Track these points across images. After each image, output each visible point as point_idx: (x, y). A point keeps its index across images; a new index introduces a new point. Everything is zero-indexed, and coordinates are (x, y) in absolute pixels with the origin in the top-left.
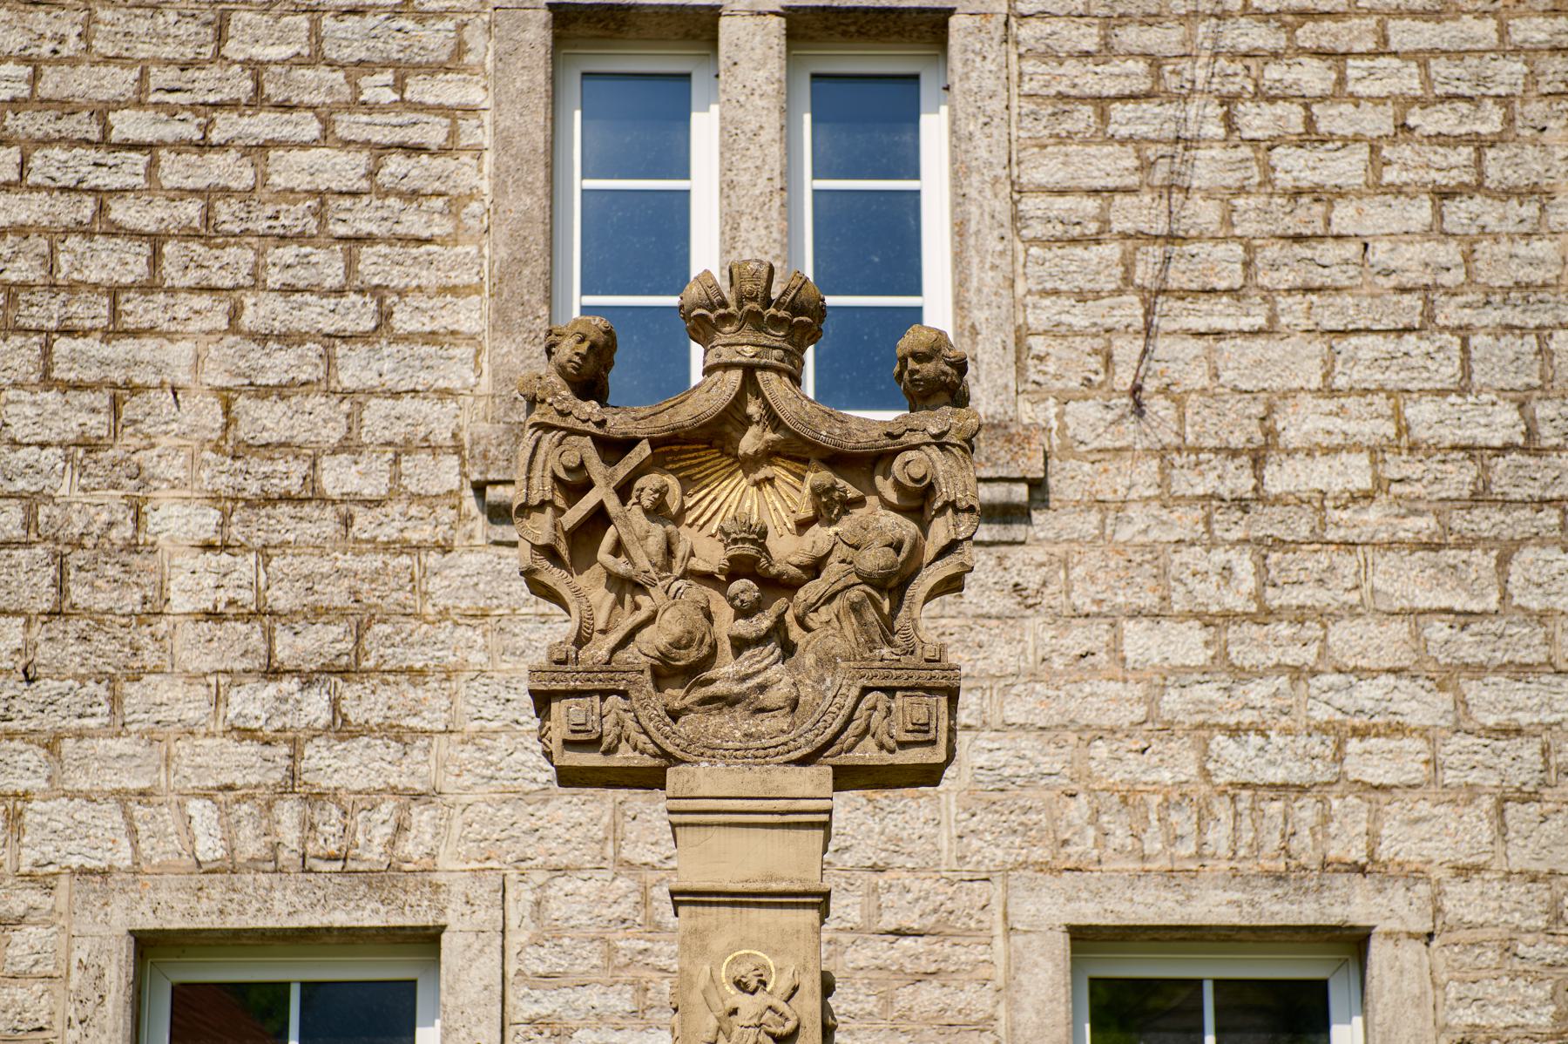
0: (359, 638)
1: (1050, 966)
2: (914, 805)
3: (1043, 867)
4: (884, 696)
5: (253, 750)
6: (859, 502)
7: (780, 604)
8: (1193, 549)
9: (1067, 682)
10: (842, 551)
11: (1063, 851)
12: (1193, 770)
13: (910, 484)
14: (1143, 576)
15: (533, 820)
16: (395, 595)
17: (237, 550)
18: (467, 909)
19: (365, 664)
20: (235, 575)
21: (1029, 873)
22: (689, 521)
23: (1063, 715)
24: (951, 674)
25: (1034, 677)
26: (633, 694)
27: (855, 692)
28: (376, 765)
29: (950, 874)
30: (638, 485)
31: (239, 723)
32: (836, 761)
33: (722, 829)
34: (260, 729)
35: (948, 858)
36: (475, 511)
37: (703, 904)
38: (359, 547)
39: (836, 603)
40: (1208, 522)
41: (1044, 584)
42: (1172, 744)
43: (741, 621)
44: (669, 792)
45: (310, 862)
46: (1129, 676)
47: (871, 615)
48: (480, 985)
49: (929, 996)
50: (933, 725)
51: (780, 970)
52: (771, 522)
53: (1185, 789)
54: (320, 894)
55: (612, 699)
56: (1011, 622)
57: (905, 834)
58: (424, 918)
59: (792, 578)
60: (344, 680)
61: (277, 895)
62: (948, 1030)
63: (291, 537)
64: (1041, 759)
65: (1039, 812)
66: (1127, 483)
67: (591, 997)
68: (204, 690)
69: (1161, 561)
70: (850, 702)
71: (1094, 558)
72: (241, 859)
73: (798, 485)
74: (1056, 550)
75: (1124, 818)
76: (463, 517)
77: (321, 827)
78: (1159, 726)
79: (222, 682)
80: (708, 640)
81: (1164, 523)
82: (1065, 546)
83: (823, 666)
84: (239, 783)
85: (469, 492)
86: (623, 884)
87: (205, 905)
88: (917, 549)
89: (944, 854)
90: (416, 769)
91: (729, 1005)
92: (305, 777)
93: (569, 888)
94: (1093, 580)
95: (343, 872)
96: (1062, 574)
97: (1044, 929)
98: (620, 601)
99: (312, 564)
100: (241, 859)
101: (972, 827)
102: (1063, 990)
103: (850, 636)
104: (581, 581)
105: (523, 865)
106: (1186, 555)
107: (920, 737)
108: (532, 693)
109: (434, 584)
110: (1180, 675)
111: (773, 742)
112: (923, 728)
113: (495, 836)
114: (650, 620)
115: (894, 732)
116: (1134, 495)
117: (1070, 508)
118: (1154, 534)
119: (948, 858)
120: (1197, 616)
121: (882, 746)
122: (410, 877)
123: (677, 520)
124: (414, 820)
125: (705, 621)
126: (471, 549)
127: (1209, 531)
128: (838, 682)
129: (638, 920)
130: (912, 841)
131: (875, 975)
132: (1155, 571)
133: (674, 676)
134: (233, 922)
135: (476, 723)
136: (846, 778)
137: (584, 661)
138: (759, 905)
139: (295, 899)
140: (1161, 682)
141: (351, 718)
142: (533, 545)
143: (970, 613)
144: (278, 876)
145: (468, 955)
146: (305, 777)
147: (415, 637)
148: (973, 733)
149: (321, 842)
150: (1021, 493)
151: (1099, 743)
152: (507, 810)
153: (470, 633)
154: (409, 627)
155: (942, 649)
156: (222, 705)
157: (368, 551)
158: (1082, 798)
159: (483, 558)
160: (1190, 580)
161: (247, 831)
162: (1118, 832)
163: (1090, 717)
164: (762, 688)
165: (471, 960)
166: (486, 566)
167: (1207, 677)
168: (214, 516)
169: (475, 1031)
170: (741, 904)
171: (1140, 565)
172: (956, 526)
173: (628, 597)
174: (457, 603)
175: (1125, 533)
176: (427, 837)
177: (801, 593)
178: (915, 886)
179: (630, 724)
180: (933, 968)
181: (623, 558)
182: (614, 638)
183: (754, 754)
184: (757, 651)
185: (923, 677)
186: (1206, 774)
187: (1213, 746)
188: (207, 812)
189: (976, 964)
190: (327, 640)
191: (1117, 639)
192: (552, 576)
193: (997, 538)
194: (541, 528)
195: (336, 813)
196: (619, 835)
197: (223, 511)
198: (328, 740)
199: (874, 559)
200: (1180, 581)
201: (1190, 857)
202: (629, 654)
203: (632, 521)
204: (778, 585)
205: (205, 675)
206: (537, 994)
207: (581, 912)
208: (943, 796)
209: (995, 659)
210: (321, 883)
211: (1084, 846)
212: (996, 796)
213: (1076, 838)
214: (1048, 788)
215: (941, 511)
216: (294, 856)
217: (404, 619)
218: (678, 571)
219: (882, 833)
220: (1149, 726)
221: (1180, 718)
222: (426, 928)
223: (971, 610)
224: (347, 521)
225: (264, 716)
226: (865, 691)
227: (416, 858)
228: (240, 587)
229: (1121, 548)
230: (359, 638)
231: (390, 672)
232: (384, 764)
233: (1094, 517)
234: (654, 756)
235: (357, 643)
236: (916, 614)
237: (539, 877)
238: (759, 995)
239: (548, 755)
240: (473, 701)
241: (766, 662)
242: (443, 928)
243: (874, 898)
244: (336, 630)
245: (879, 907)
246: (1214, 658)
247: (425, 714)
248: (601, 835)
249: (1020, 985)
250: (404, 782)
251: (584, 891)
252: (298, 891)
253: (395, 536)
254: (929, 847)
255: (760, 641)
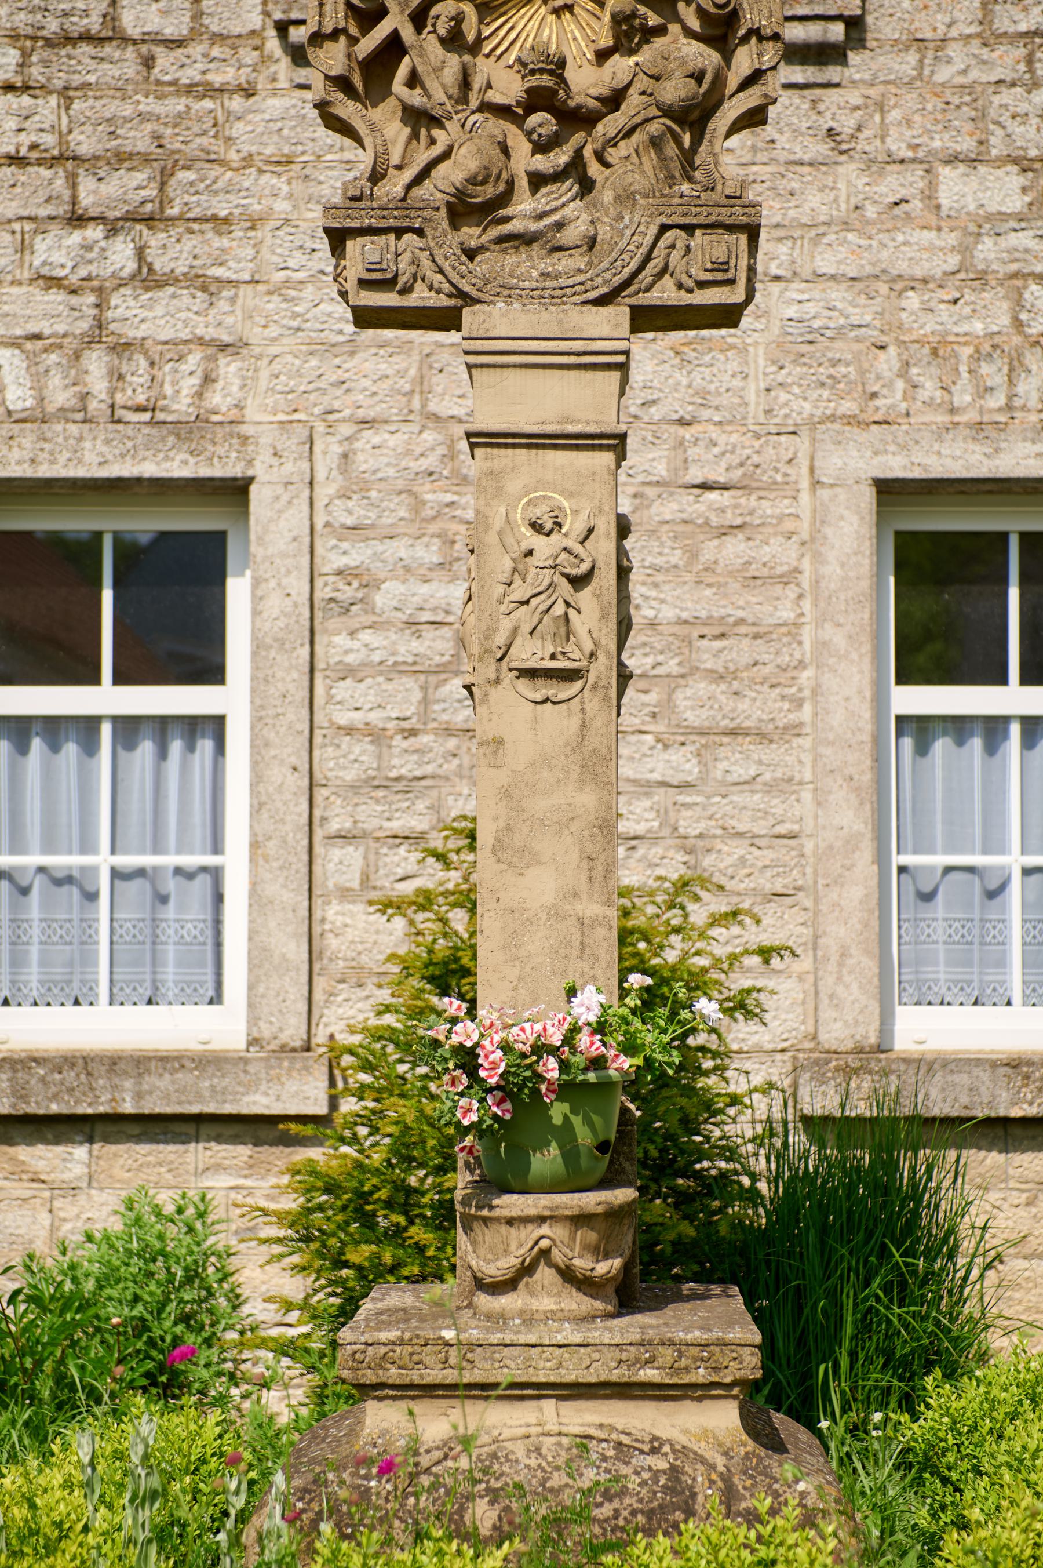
0: (163, 184)
1: (855, 519)
2: (721, 357)
3: (851, 420)
4: (683, 234)
5: (60, 298)
6: (661, 31)
7: (579, 137)
8: (1013, 90)
9: (880, 231)
10: (643, 82)
11: (871, 404)
12: (1005, 320)
13: (713, 10)
14: (960, 121)
15: (340, 372)
16: (198, 140)
17: (38, 92)
18: (275, 461)
19: (170, 212)
20: (37, 118)
21: (837, 426)
22: (486, 51)
23: (874, 265)
24: (752, 211)
25: (846, 226)
26: (429, 232)
27: (654, 230)
28: (183, 315)
29: (756, 428)
30: (433, 12)
31: (45, 271)
32: (633, 301)
33: (518, 371)
34: (66, 277)
35: (755, 411)
36: (278, 52)
37: (499, 445)
38: (161, 89)
39: (636, 138)
40: (1030, 60)
41: (859, 129)
42: (985, 295)
43: (539, 156)
44: (464, 332)
45: (120, 413)
46: (943, 224)
47: (671, 150)
48: (288, 536)
49: (734, 548)
50: (732, 264)
51: (576, 512)
52: (571, 52)
53: (997, 340)
54: (129, 444)
55: (408, 237)
56: (824, 168)
57: (712, 387)
58: (235, 470)
59: (590, 111)
60: (150, 228)
61: (87, 444)
62: (752, 583)
63: (92, 78)
64: (851, 310)
65: (848, 365)
66: (948, 20)
67: (399, 549)
68: (8, 237)
69: (980, 102)
70: (648, 240)
71: (910, 100)
72: (50, 408)
73: (598, 12)
74: (872, 92)
75: (934, 370)
76: (267, 59)
77: (129, 378)
78: (972, 276)
79: (27, 228)
80: (504, 176)
81: (984, 62)
82: (881, 88)
83: (621, 206)
84: (47, 332)
85: (272, 33)
86: (429, 437)
87: (16, 454)
88: (719, 80)
89: (752, 408)
90: (222, 320)
91: (525, 546)
92: (112, 327)
93: (376, 440)
94: (909, 123)
95: (151, 423)
96: (877, 118)
97: (851, 482)
98: (415, 136)
99: (114, 107)
100: (50, 408)
101: (780, 379)
102: (867, 543)
103: (650, 172)
104: (376, 114)
105: (331, 417)
106: (1007, 96)
107: (719, 276)
108: (327, 230)
109: (238, 129)
110: (995, 222)
111: (570, 282)
112: (722, 267)
113: (302, 388)
114: (446, 155)
115: (693, 271)
116: (954, 33)
117: (888, 48)
118: (974, 74)
119: (755, 411)
120: (1015, 161)
121: (680, 286)
122: (218, 429)
123: (475, 48)
124: (222, 371)
125: (502, 157)
126: (275, 92)
127: (1031, 70)
128: (636, 220)
129: (445, 473)
130: (719, 394)
131: (680, 528)
132: (973, 114)
133: (470, 213)
134: (45, 471)
135: (282, 273)
136: (647, 319)
137: (379, 198)
138: (555, 447)
139: (105, 449)
140: (976, 230)
141: (157, 266)
142: (327, 77)
143: (782, 159)
144: (87, 426)
145: (278, 506)
146: (112, 327)
147: (220, 184)
148: (783, 284)
149: (129, 392)
150: (837, 31)
151: (911, 293)
152: (314, 362)
153: (274, 181)
154: (213, 174)
155: (743, 185)
156: (27, 252)
157: (170, 94)
158: (892, 350)
159: (286, 102)
160: (1009, 123)
161: (56, 380)
162: (928, 385)
163: (902, 267)
164: (559, 226)
165: (280, 511)
166: (283, 109)
167: (1023, 225)
168: (13, 56)
169: (284, 581)
170: (537, 446)
171: (958, 107)
172: (760, 55)
173: (423, 132)
174: (261, 149)
175: (944, 74)
176: (235, 389)
177: (600, 127)
178: (722, 439)
179: (426, 263)
180: (738, 521)
181: (418, 90)
182: (409, 174)
183: (551, 293)
184: (554, 187)
185: (723, 214)
186: (1018, 324)
187: (1027, 295)
188: (16, 361)
189: (781, 518)
190: (129, 187)
191: (932, 186)
192: (347, 109)
193: (812, 80)
194: (333, 58)
195: (143, 363)
196: (426, 388)
197: (22, 49)
198: (134, 288)
199: (675, 90)
200: (998, 123)
201: (1000, 409)
202: (425, 191)
203: (427, 51)
204: (577, 119)
205: (10, 221)
206: (345, 545)
207: (388, 464)
208: (751, 349)
209: (807, 207)
210: (130, 433)
211: (893, 399)
212: (805, 348)
213: (885, 391)
214: (857, 340)
215: (745, 40)
216: (103, 406)
217: (208, 165)
218: (474, 104)
219: (689, 386)
220: (962, 275)
221: (994, 267)
222: (235, 479)
223: (783, 156)
224: (148, 62)
225: (70, 264)
226: (664, 228)
227: (224, 409)
228: (42, 130)
229: (939, 89)
230: (163, 184)
231: (195, 220)
232: (191, 315)
233: (912, 57)
234: (450, 296)
235: (161, 190)
236: (717, 149)
237: (346, 430)
238: (554, 537)
239: (343, 294)
240: (279, 251)
241: (564, 199)
242: (251, 480)
243: (680, 451)
244: (140, 177)
245: (686, 461)
246: (1031, 204)
247: (231, 264)
248: (407, 387)
249: (825, 538)
250: (210, 333)
251: (391, 444)
252: (108, 442)
253: (198, 78)
254: (737, 400)
255: (558, 177)
